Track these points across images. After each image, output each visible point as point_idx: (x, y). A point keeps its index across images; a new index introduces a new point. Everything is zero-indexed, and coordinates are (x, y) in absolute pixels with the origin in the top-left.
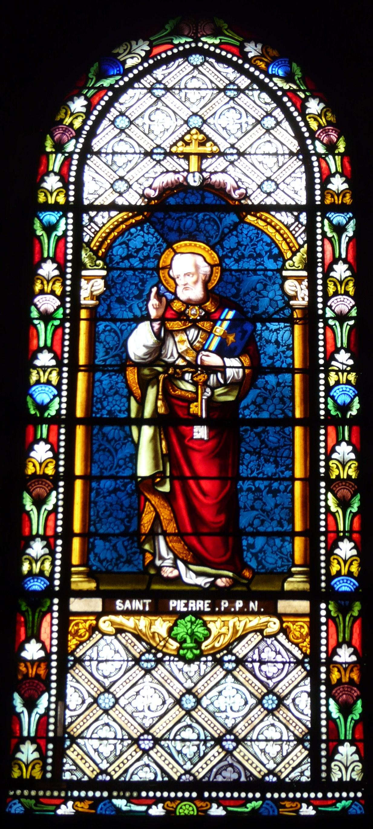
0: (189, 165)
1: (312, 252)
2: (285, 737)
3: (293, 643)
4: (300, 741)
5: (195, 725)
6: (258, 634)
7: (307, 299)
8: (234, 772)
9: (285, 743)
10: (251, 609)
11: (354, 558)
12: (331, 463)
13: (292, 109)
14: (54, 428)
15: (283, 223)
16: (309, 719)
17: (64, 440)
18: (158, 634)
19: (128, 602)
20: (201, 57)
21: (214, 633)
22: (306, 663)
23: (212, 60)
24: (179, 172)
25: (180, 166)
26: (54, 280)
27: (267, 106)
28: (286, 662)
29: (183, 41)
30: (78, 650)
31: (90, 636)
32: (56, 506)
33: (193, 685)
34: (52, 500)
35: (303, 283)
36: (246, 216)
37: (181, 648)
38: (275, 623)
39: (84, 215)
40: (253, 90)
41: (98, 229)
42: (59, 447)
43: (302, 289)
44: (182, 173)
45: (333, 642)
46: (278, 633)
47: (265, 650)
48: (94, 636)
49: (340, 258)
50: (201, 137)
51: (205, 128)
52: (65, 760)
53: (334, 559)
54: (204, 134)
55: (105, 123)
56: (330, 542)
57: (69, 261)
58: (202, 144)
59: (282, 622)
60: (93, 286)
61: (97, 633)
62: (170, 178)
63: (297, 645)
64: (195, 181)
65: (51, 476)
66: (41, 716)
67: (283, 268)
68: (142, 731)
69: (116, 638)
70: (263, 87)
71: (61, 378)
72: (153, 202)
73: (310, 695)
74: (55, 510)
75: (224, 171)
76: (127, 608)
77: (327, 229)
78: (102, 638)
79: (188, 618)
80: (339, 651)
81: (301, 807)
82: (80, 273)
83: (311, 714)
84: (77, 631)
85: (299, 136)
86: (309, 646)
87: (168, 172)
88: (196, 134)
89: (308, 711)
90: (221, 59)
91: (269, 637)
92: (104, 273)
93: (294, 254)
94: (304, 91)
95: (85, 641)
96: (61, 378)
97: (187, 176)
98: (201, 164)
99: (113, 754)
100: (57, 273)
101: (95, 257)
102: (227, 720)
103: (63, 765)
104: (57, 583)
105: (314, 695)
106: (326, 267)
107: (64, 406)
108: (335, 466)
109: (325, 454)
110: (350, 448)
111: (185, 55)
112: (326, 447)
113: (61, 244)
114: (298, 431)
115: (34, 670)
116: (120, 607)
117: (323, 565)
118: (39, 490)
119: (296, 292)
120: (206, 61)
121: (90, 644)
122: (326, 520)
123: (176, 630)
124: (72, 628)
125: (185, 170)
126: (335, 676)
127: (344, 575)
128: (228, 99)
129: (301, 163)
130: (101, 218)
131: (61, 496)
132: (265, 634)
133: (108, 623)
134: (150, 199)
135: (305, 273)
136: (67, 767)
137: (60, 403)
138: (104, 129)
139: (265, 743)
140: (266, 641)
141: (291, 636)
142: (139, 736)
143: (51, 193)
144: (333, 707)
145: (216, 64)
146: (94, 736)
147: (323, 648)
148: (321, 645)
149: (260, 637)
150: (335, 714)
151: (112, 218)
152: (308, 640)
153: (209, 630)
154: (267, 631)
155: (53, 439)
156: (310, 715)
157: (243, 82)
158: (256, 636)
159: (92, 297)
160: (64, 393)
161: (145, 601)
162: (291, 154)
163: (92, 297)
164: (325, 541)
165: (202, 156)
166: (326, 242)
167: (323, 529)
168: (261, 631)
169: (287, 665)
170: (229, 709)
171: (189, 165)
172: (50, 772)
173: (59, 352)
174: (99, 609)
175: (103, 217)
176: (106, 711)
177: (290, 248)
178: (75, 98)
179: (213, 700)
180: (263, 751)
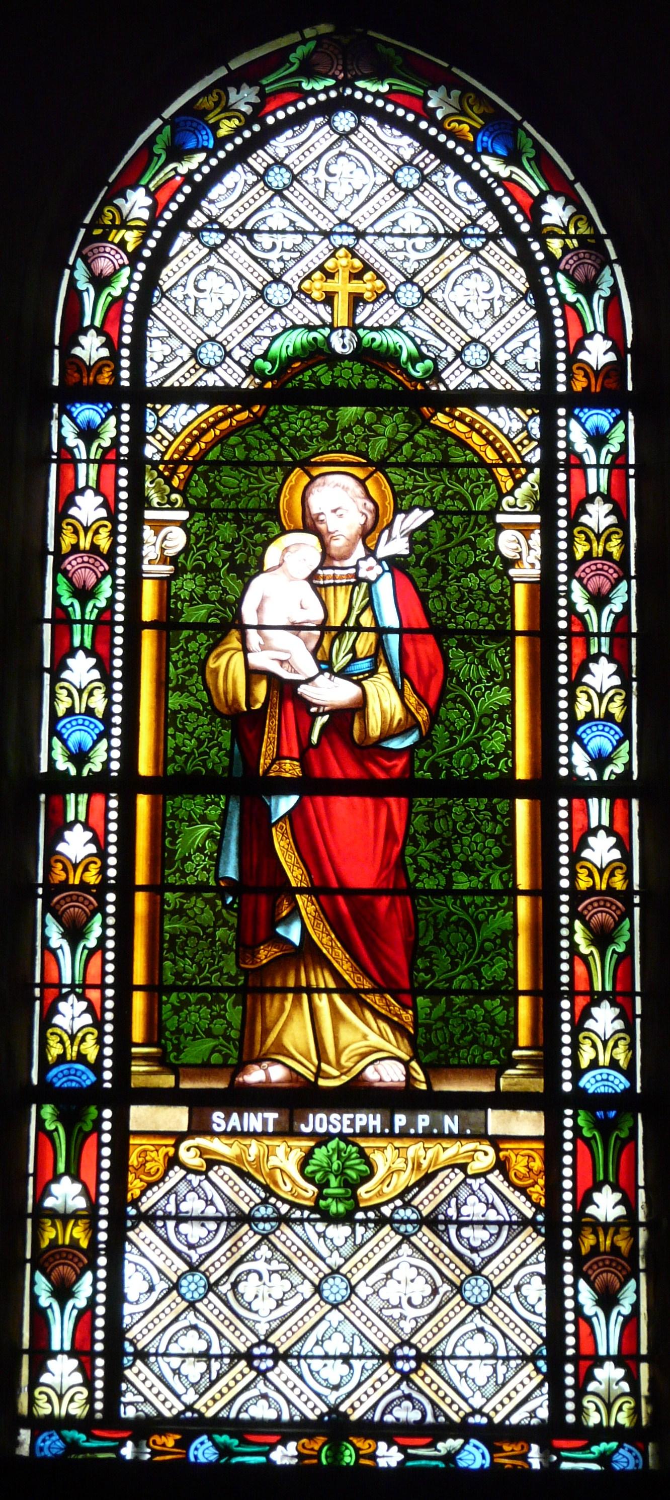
0: (332, 315)
1: (547, 484)
3: (516, 1188)
6: (457, 1170)
8: (414, 1408)
9: (501, 1361)
10: (447, 1132)
11: (613, 529)
14: (98, 800)
16: (544, 1322)
17: (101, 1341)
18: (282, 1171)
19: (235, 1116)
21: (380, 1173)
23: (371, 122)
24: (313, 328)
25: (318, 315)
26: (101, 363)
27: (471, 207)
28: (504, 1223)
29: (319, 86)
30: (144, 1199)
31: (166, 1174)
32: (102, 939)
33: (342, 1261)
35: (532, 536)
36: (434, 415)
37: (321, 1196)
38: (486, 1154)
41: (171, 438)
42: (118, 500)
43: (530, 548)
44: (321, 330)
45: (586, 1182)
48: (171, 1173)
51: (363, 247)
52: (150, 323)
53: (585, 1038)
56: (583, 1371)
58: (357, 276)
59: (498, 1151)
60: (165, 539)
61: (177, 1168)
62: (299, 338)
63: (523, 1190)
64: (344, 346)
65: (94, 886)
67: (497, 509)
69: (208, 1179)
71: (110, 703)
72: (269, 385)
73: (545, 1279)
74: (123, 299)
75: (395, 326)
76: (234, 1128)
77: (580, 937)
79: (333, 1144)
80: (596, 1196)
81: (530, 1449)
82: (143, 514)
83: (547, 1313)
86: (543, 1192)
87: (295, 327)
88: (346, 256)
89: (542, 1308)
90: (385, 119)
91: (475, 1176)
92: (184, 515)
93: (517, 484)
95: (156, 1183)
96: (110, 703)
97: (330, 335)
101: (167, 488)
104: (107, 1075)
106: (574, 507)
107: (116, 754)
109: (571, 1202)
111: (328, 109)
114: (522, 807)
116: (219, 1125)
118: (75, 910)
119: (520, 553)
121: (165, 1187)
122: (576, 1334)
125: (324, 325)
126: (589, 1241)
128: (402, 311)
129: (533, 312)
131: (111, 921)
132: (470, 1172)
133: (193, 1151)
134: (265, 378)
135: (537, 519)
136: (128, 1397)
137: (109, 749)
141: (512, 1174)
144: (587, 1295)
146: (174, 1349)
147: (564, 837)
150: (590, 1308)
152: (541, 1182)
155: (96, 820)
156: (544, 1315)
158: (452, 1175)
160: (116, 731)
161: (266, 1115)
165: (356, 300)
166: (578, 961)
168: (463, 1167)
169: (506, 1228)
171: (332, 315)
173: (100, 831)
174: (184, 1128)
176: (192, 1305)
178: (129, 192)
179: (377, 1286)
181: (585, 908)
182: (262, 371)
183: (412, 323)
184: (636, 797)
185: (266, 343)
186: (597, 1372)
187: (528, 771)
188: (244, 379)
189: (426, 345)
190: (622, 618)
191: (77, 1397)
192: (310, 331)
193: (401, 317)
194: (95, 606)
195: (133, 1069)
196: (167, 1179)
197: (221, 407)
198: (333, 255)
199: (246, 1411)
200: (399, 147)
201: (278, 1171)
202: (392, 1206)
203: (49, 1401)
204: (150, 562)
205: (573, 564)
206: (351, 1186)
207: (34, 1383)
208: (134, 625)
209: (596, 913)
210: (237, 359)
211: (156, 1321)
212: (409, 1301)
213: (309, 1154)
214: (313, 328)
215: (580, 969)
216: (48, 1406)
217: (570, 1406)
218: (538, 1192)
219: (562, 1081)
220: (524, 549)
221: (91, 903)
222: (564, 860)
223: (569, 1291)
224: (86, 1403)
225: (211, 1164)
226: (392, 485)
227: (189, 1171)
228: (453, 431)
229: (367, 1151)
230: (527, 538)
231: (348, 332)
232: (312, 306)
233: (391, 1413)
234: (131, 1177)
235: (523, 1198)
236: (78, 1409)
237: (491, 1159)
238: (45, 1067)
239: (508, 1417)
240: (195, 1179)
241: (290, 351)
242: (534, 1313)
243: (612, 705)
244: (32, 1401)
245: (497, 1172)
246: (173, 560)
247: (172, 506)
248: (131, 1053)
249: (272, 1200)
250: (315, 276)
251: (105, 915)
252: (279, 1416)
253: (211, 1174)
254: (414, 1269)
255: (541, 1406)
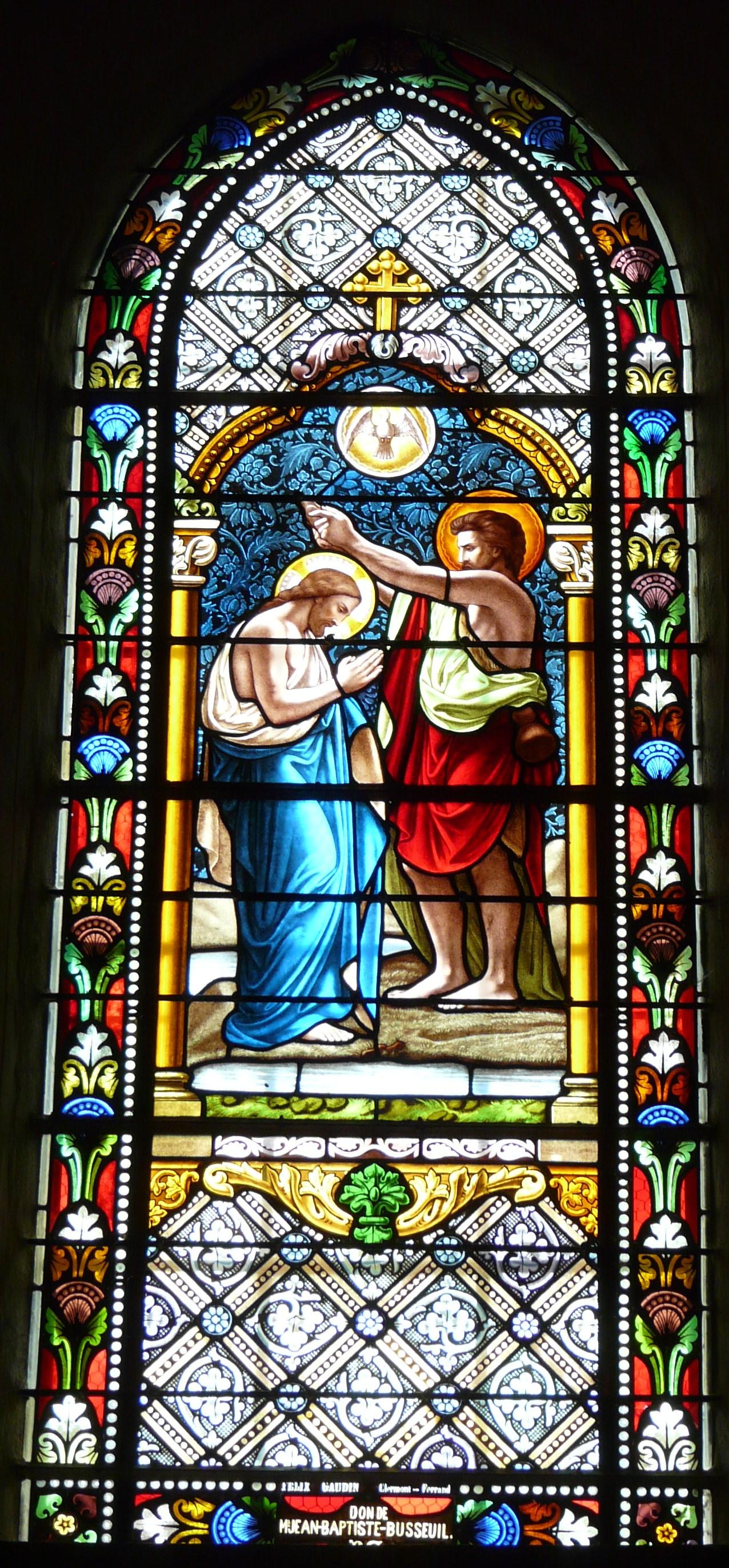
0: (374, 319)
2: (551, 1391)
3: (568, 1216)
4: (580, 1399)
5: (398, 152)
6: (504, 1199)
7: (591, 578)
12: (640, 1447)
13: (568, 212)
15: (547, 431)
16: (596, 1359)
17: (140, 872)
18: (314, 1197)
20: (397, 115)
21: (422, 1198)
22: (593, 1398)
24: (356, 332)
26: (121, 540)
27: (520, 208)
30: (165, 1227)
31: (189, 1199)
34: (130, 605)
37: (355, 1224)
38: (534, 1180)
39: (178, 415)
40: (494, 175)
41: (207, 438)
46: (541, 1198)
47: (517, 1229)
48: (195, 1199)
49: (661, 847)
50: (398, 265)
51: (407, 250)
52: (183, 327)
54: (405, 260)
55: (219, 237)
56: (629, 515)
57: (156, 346)
59: (548, 1177)
61: (201, 1194)
63: (575, 1220)
64: (384, 351)
66: (133, 463)
68: (284, 1377)
69: (237, 1206)
70: (510, 167)
72: (307, 389)
74: (141, 459)
75: (439, 331)
78: (209, 1204)
79: (370, 1170)
82: (172, 524)
84: (163, 1191)
85: (577, 259)
87: (334, 330)
89: (594, 1344)
90: (435, 119)
92: (215, 524)
94: (588, 175)
95: (178, 1210)
96: (121, 1084)
98: (399, 317)
99: (228, 1420)
100: (127, 526)
102: (442, 1359)
103: (137, 1440)
104: (129, 1103)
105: (607, 1316)
108: (649, 1453)
110: (679, 1414)
111: (369, 109)
112: (627, 862)
113: (106, 1178)
115: (113, 553)
117: (623, 1084)
119: (572, 566)
120: (405, 121)
121: (188, 1215)
123: (350, 1190)
124: (154, 1186)
125: (366, 328)
126: (646, 1277)
127: (666, 1288)
129: (584, 316)
130: (214, 417)
132: (517, 1200)
133: (221, 1175)
134: (302, 383)
135: (588, 529)
136: (143, 1446)
138: (217, 250)
139: (512, 1403)
140: (520, 1213)
141: (564, 1203)
142: (278, 1387)
143: (90, 1070)
145: (425, 129)
148: (619, 1372)
149: (508, 1205)
150: (644, 975)
151: (234, 418)
152: (595, 1212)
153: (409, 1192)
154: (518, 1197)
157: (476, 160)
158: (499, 1204)
159: (194, 568)
162: (566, 295)
163: (194, 568)
164: (627, 1040)
165: (400, 301)
167: (624, 1391)
170: (445, 1339)
172: (114, 1438)
175: (216, 417)
177: (563, 480)
180: (509, 1417)
181: (649, 1303)
182: (300, 375)
183: (458, 327)
184: (696, 802)
185: (304, 347)
186: (639, 346)
187: (582, 634)
188: (279, 384)
189: (472, 350)
190: (686, 987)
191: (85, 1445)
192: (350, 336)
193: (447, 321)
194: (120, 622)
195: (156, 1095)
196: (190, 1205)
197: (258, 409)
198: (376, 257)
199: (273, 1458)
200: (447, 146)
201: (311, 1198)
202: (434, 1235)
203: (55, 1449)
204: (181, 572)
205: (628, 576)
206: (389, 1216)
207: (40, 1428)
208: (162, 640)
209: (661, 1309)
210: (274, 364)
211: (173, 1433)
212: (450, 1336)
213: (347, 1180)
214: (356, 332)
215: (630, 475)
216: (53, 1454)
217: (624, 1450)
218: (591, 1221)
219: (619, 1385)
220: (576, 561)
221: (113, 929)
222: (623, 1071)
223: (624, 1326)
224: (95, 1451)
225: (239, 1190)
226: (436, 420)
227: (214, 1197)
228: (502, 436)
229: (407, 1177)
230: (580, 550)
231: (391, 337)
232: (351, 310)
233: (429, 1459)
234: (152, 1203)
235: (575, 1227)
236: (86, 1457)
237: (540, 1185)
238: (60, 1099)
239: (556, 1463)
240: (222, 1206)
241: (330, 353)
242: (586, 1350)
243: (665, 556)
244: (36, 1449)
245: (547, 1199)
246: (204, 571)
247: (203, 514)
248: (154, 1078)
249: (305, 1229)
250: (357, 278)
251: (147, 429)
252: (309, 1464)
253: (239, 1200)
254: (457, 1303)
255: (593, 1451)
